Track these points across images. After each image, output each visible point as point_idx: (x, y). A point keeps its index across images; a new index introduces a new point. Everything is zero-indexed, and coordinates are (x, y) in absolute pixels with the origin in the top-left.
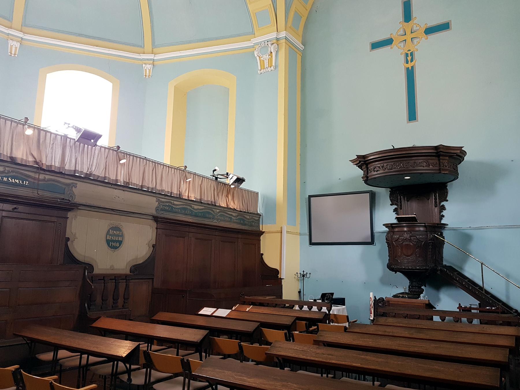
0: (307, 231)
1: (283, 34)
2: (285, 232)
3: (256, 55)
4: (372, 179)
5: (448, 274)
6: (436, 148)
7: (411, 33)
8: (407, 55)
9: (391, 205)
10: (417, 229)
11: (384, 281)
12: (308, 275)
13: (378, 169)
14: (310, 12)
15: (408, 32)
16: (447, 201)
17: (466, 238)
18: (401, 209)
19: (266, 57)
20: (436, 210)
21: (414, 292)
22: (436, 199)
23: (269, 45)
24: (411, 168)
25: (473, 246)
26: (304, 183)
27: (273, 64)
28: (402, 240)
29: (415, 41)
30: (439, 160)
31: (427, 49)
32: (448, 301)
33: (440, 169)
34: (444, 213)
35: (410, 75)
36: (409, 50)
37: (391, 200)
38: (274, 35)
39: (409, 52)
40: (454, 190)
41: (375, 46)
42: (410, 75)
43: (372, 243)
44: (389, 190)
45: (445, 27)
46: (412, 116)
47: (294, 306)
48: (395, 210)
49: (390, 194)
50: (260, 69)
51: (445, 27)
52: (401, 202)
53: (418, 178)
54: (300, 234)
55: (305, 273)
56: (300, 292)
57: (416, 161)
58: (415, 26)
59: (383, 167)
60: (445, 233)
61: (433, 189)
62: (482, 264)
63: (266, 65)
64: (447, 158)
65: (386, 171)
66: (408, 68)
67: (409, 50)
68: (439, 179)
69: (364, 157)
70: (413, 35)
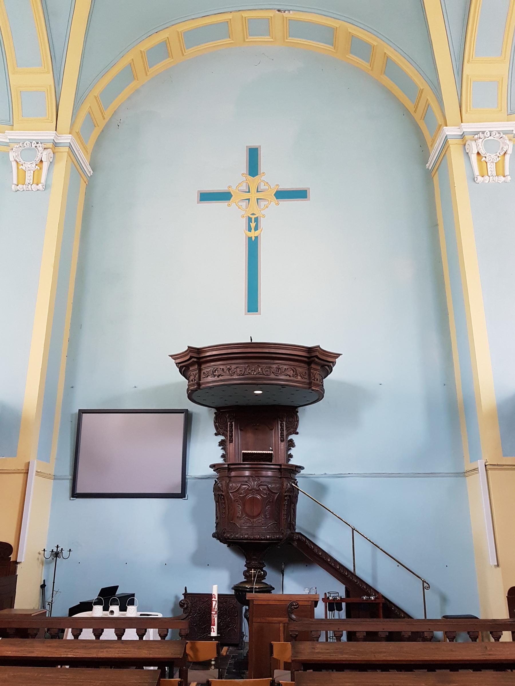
0: (67, 472)
1: (66, 139)
2: (34, 473)
3: (12, 159)
4: (207, 388)
5: (307, 545)
6: (310, 350)
7: (257, 191)
8: (250, 220)
9: (216, 434)
10: (264, 473)
11: (200, 560)
12: (65, 553)
13: (221, 372)
14: (107, 125)
15: (253, 190)
16: (297, 433)
17: (321, 489)
18: (231, 441)
19: (30, 166)
20: (282, 446)
21: (254, 576)
23: (40, 149)
24: (273, 376)
26: (70, 387)
27: (43, 180)
28: (245, 492)
29: (262, 203)
30: (309, 369)
31: (276, 217)
32: (294, 584)
33: (310, 384)
34: (293, 451)
35: (253, 247)
36: (253, 214)
37: (216, 426)
38: (49, 135)
39: (253, 217)
40: (308, 417)
41: (206, 197)
42: (253, 247)
43: (182, 495)
44: (214, 410)
45: (301, 194)
46: (253, 305)
47: (63, 631)
48: (222, 443)
49: (216, 418)
50: (15, 182)
51: (301, 194)
52: (231, 431)
53: (258, 393)
54: (55, 478)
55: (59, 549)
56: (43, 586)
57: (281, 366)
58: (262, 184)
59: (229, 369)
61: (281, 416)
62: (353, 529)
63: (29, 178)
65: (235, 377)
66: (250, 238)
67: (253, 214)
69: (199, 351)
70: (260, 195)
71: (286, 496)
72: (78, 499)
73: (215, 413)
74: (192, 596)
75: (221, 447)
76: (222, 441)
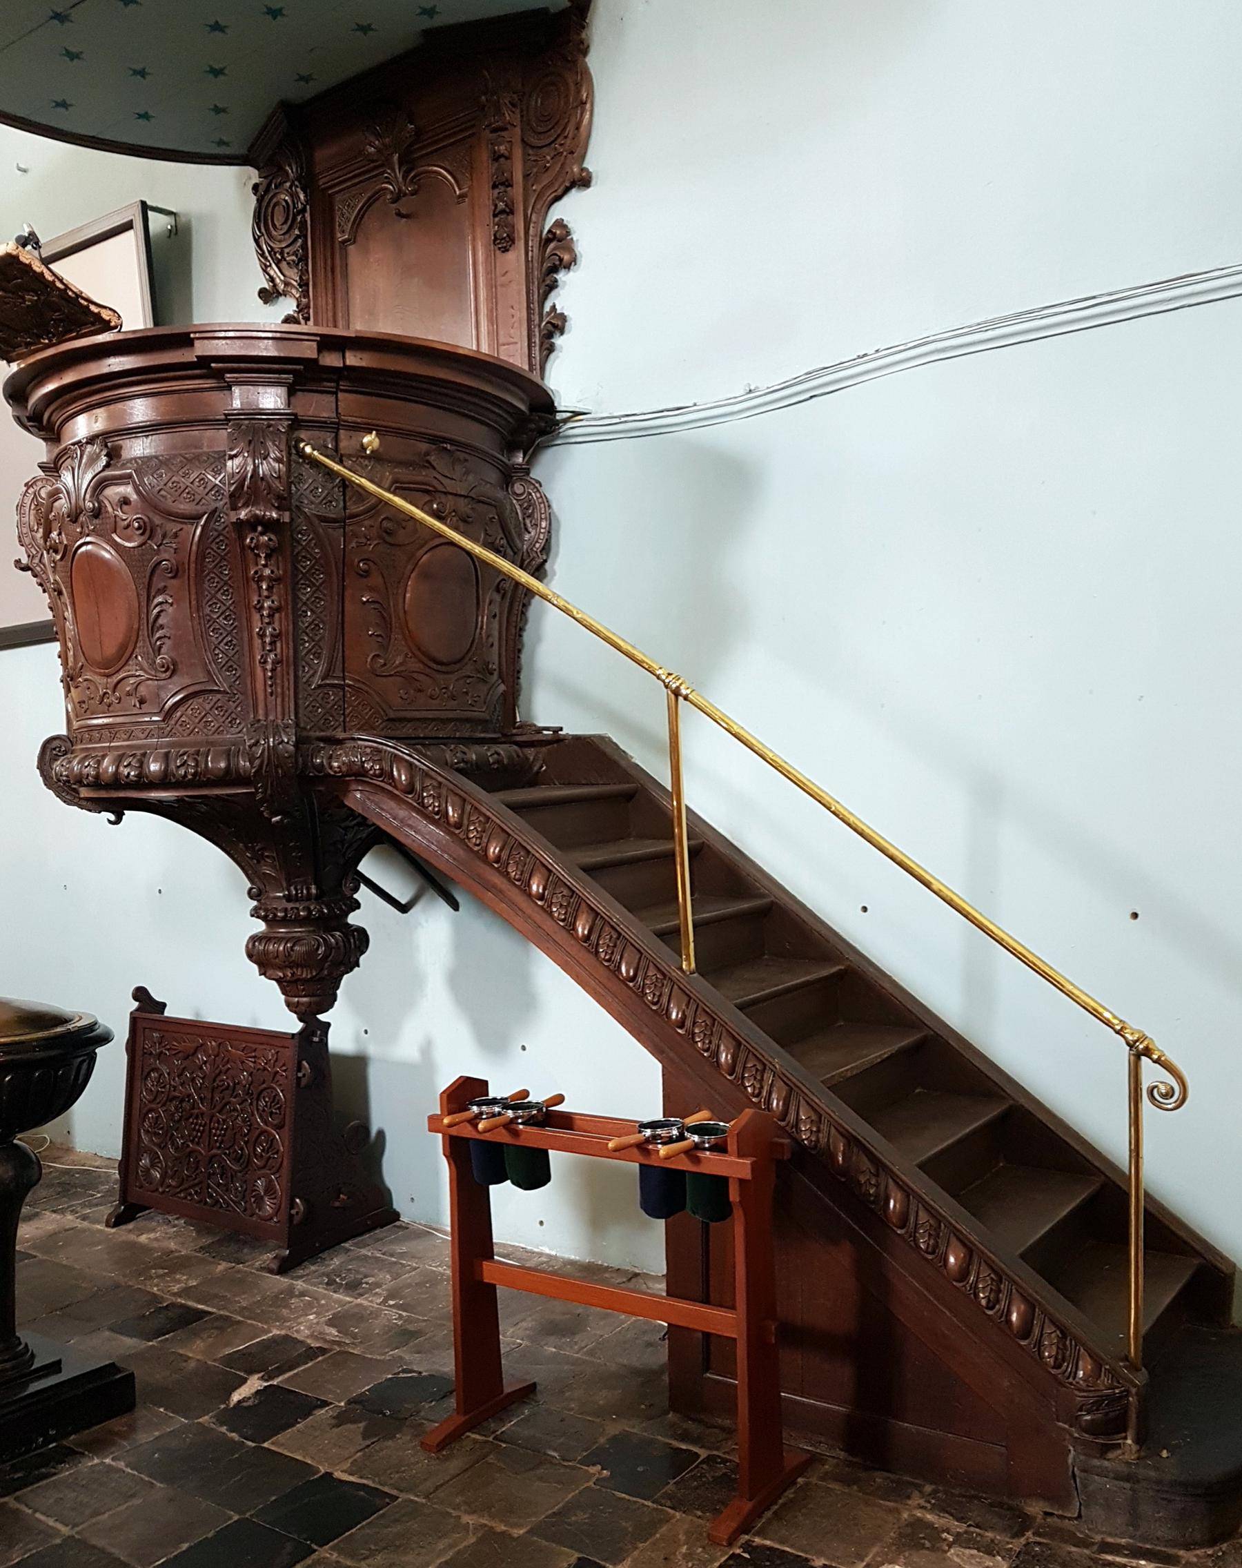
16: (584, 182)
17: (724, 486)
25: (770, 556)
34: (569, 295)
60: (576, 485)
73: (256, 188)
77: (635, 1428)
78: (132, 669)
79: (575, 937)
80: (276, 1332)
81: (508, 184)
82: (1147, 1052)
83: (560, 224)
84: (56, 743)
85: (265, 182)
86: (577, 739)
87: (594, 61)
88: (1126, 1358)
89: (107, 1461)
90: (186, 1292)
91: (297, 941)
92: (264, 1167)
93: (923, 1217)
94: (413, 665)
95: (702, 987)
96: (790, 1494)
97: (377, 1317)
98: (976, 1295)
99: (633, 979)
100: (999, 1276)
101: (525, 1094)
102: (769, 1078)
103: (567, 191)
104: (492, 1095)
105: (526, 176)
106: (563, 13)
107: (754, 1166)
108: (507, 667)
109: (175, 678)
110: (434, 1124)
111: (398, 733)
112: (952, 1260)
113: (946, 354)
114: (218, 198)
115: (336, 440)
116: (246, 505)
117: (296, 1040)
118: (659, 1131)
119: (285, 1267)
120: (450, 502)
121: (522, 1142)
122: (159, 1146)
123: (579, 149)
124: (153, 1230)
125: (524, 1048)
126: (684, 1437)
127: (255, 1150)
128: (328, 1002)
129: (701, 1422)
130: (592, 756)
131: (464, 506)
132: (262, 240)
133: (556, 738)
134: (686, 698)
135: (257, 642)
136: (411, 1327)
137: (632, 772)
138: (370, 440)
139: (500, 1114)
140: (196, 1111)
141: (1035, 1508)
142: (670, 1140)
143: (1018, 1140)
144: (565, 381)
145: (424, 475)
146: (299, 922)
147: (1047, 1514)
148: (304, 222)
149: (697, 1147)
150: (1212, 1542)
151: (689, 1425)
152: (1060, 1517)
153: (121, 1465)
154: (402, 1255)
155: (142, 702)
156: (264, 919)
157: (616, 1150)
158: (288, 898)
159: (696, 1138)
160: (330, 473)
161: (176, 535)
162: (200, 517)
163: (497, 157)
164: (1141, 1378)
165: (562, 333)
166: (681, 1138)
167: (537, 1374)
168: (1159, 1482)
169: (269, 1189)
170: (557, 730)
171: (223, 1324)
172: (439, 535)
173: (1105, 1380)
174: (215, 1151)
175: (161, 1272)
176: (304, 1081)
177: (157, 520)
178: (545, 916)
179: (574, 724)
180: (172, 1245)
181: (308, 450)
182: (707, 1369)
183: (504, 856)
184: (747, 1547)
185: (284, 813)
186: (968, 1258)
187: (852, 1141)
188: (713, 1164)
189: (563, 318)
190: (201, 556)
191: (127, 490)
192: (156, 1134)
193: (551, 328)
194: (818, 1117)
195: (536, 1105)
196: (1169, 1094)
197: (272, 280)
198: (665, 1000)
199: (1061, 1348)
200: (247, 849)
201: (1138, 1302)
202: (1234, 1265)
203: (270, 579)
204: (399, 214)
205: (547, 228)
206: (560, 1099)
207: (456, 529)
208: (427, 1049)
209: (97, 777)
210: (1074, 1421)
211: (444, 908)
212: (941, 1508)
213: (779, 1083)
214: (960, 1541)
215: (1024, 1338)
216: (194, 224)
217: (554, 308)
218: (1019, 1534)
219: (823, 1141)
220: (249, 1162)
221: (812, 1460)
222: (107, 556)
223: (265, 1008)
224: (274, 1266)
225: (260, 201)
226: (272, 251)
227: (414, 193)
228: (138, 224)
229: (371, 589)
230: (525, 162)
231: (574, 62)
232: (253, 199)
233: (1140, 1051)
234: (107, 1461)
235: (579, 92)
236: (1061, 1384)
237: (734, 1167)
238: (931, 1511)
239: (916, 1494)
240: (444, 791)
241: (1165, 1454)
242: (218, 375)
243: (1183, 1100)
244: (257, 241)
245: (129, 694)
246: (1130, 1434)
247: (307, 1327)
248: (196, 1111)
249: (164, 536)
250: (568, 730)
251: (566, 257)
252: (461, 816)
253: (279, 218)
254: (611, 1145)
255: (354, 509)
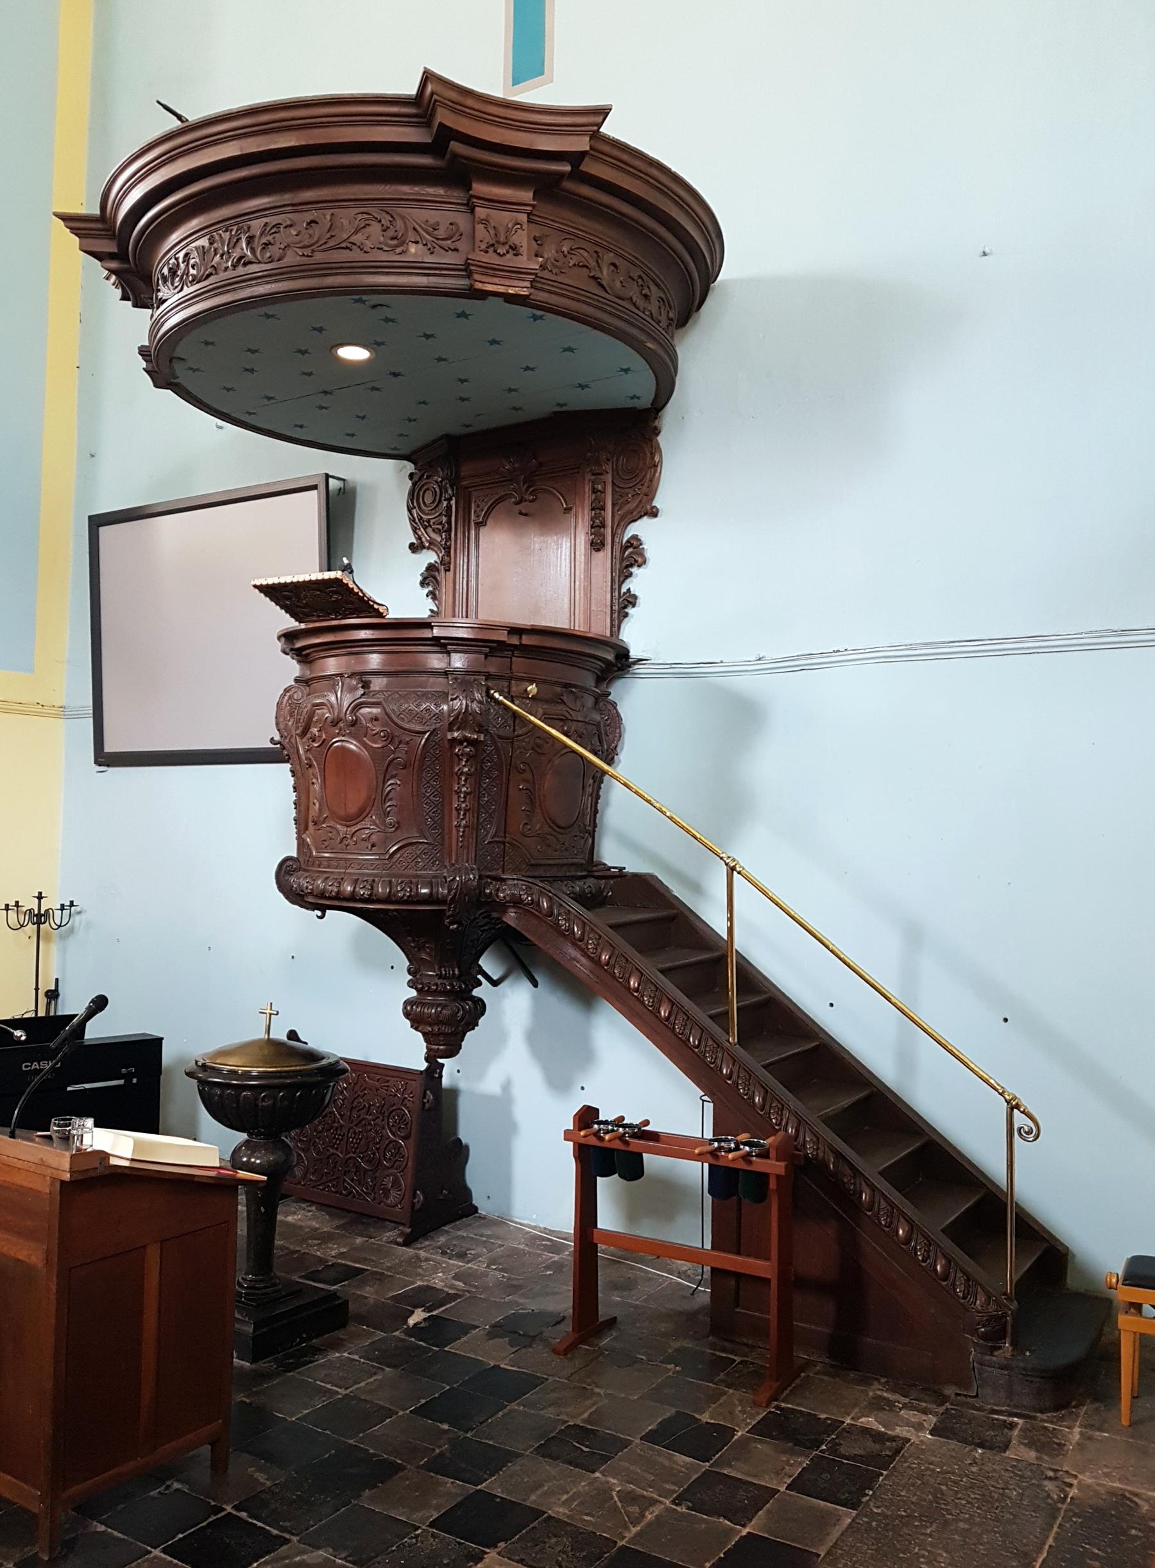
9: (414, 548)
16: (654, 513)
17: (738, 718)
22: (597, 507)
25: (769, 766)
34: (639, 582)
60: (633, 700)
64: (527, 196)
68: (604, 372)
71: (460, 742)
72: (111, 770)
73: (411, 476)
74: (375, 1070)
75: (426, 591)
76: (431, 568)
77: (688, 1344)
78: (367, 823)
79: (658, 1018)
80: (419, 1283)
81: (603, 508)
82: (1017, 1107)
83: (635, 537)
84: (288, 863)
85: (419, 474)
86: (636, 876)
87: (661, 439)
88: (1005, 1294)
89: (346, 1354)
90: (341, 1255)
91: (444, 1007)
92: (392, 1167)
93: (883, 1204)
94: (547, 829)
95: (740, 1052)
96: (797, 1381)
97: (487, 1276)
98: (916, 1254)
99: (698, 1047)
100: (929, 1242)
101: (622, 1118)
102: (786, 1114)
103: (641, 517)
104: (602, 1118)
105: (613, 505)
106: (647, 411)
107: (786, 1167)
108: (586, 825)
109: (398, 832)
110: (568, 1135)
111: (536, 874)
112: (901, 1232)
113: (889, 659)
114: (383, 483)
115: (509, 687)
116: (458, 730)
117: (424, 1075)
118: (722, 1144)
119: (408, 1242)
120: (574, 726)
121: (630, 1149)
122: (303, 1150)
123: (651, 494)
124: (295, 1213)
125: (583, 1088)
126: (724, 1350)
127: (385, 1154)
128: (453, 1051)
129: (732, 1341)
130: (643, 889)
131: (581, 727)
132: (414, 511)
133: (621, 874)
134: (739, 873)
135: (455, 813)
136: (515, 1283)
137: (675, 902)
138: (532, 689)
139: (613, 1131)
140: (336, 1125)
141: (950, 1391)
142: (730, 1150)
143: (934, 1163)
144: (636, 635)
145: (560, 709)
146: (444, 993)
147: (957, 1394)
148: (449, 507)
149: (749, 1154)
150: (1056, 1410)
151: (726, 1344)
152: (965, 1396)
153: (356, 1357)
154: (488, 1236)
155: (373, 846)
156: (416, 989)
157: (700, 1154)
158: (440, 977)
159: (747, 1148)
160: (507, 708)
161: (407, 743)
162: (425, 733)
163: (595, 491)
164: (1014, 1306)
165: (634, 606)
166: (737, 1149)
167: (613, 1312)
168: (1024, 1369)
169: (396, 1183)
170: (621, 869)
171: (380, 1277)
172: (566, 746)
173: (992, 1307)
174: (351, 1155)
175: (316, 1242)
176: (427, 1105)
177: (397, 732)
178: (637, 1003)
179: (633, 865)
180: (315, 1224)
181: (497, 695)
182: (737, 1306)
183: (612, 962)
184: (777, 1407)
185: (460, 924)
186: (915, 1227)
187: (839, 1155)
188: (760, 1165)
189: (635, 597)
190: (423, 757)
191: (375, 711)
192: (301, 1141)
193: (624, 603)
194: (817, 1138)
195: (630, 1126)
196: (1030, 1132)
197: (420, 538)
198: (719, 1061)
199: (967, 1286)
200: (414, 941)
201: (1013, 1267)
202: (1067, 1248)
203: (467, 774)
204: (521, 513)
205: (625, 539)
206: (647, 1123)
207: (576, 742)
208: (507, 1087)
209: (338, 893)
210: (974, 1332)
211: (527, 984)
212: (894, 1391)
213: (792, 1118)
214: (905, 1406)
215: (945, 1280)
216: (358, 489)
217: (629, 590)
218: (942, 1404)
219: (821, 1155)
220: (380, 1162)
221: (808, 1364)
222: (353, 747)
223: (407, 1050)
224: (400, 1240)
225: (414, 485)
226: (421, 519)
227: (531, 501)
228: (322, 487)
229: (525, 781)
230: (613, 495)
231: (651, 440)
232: (410, 483)
233: (1013, 1106)
234: (346, 1354)
235: (653, 458)
236: (966, 1310)
237: (774, 1167)
238: (887, 1391)
239: (876, 1383)
240: (572, 917)
241: (1028, 1354)
242: (444, 646)
243: (1037, 1137)
244: (410, 510)
245: (363, 840)
246: (1008, 1340)
247: (439, 1280)
248: (336, 1125)
249: (400, 742)
250: (630, 869)
251: (640, 560)
252: (583, 933)
253: (428, 498)
254: (697, 1151)
255: (519, 732)
